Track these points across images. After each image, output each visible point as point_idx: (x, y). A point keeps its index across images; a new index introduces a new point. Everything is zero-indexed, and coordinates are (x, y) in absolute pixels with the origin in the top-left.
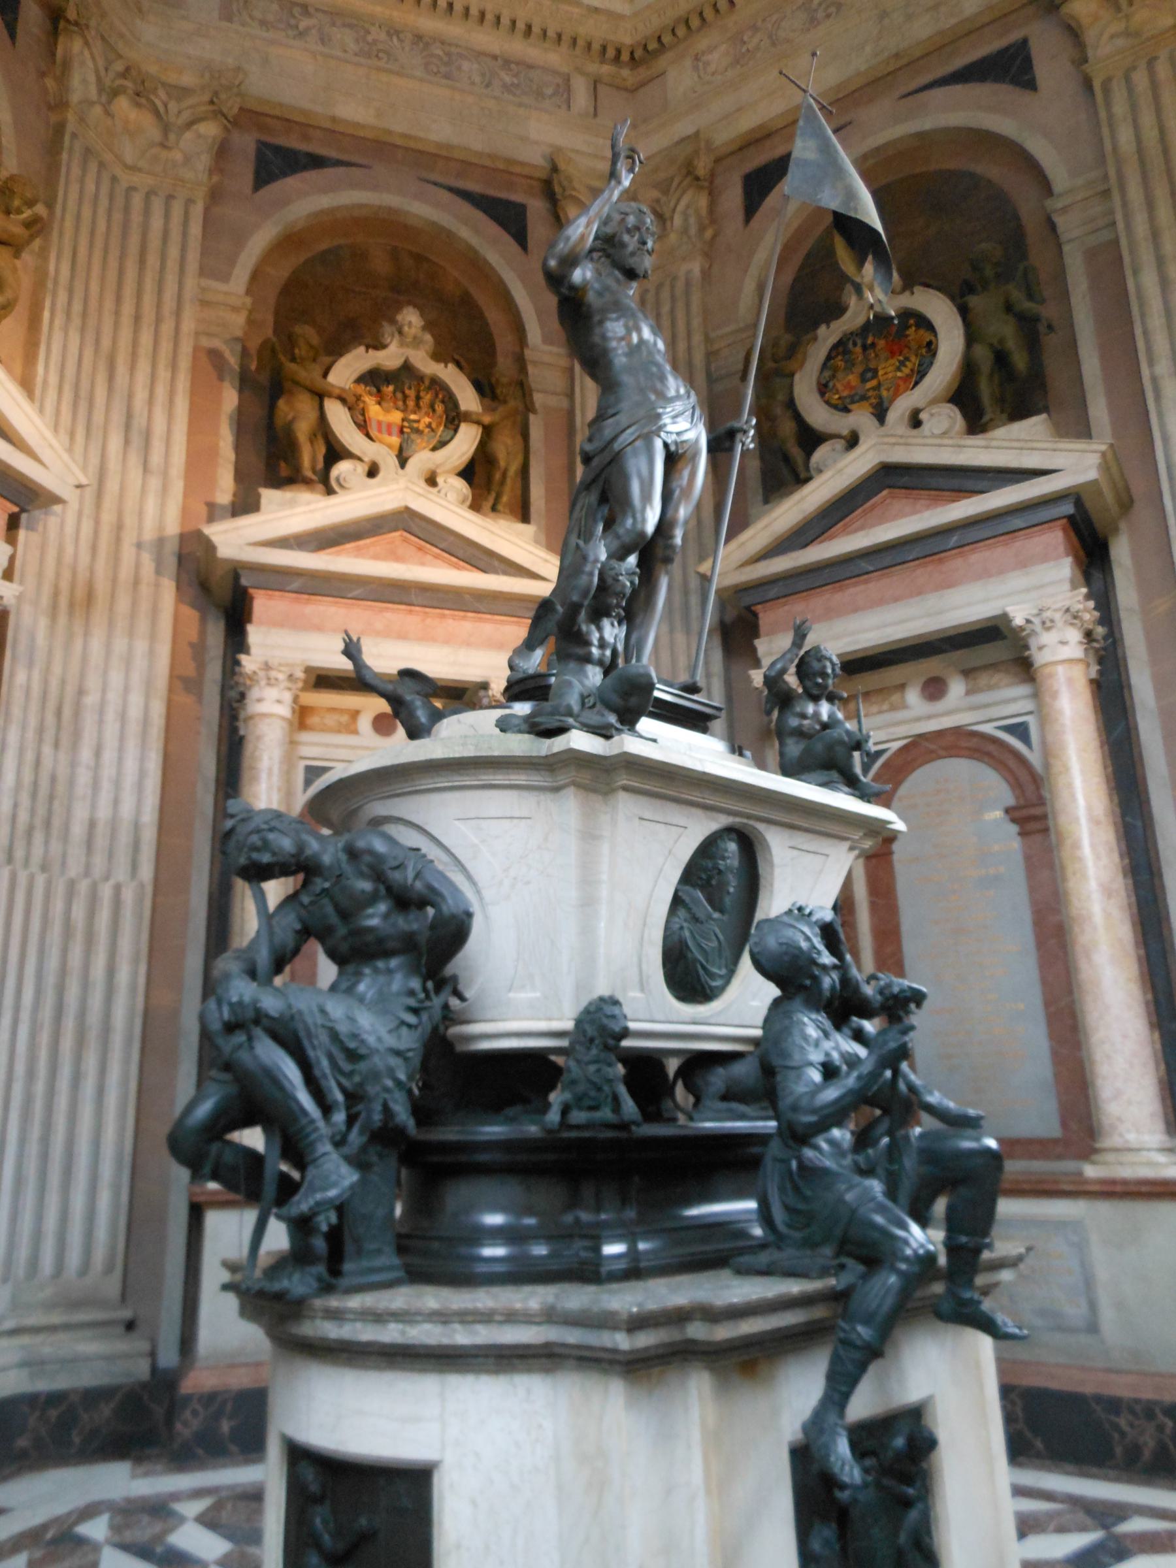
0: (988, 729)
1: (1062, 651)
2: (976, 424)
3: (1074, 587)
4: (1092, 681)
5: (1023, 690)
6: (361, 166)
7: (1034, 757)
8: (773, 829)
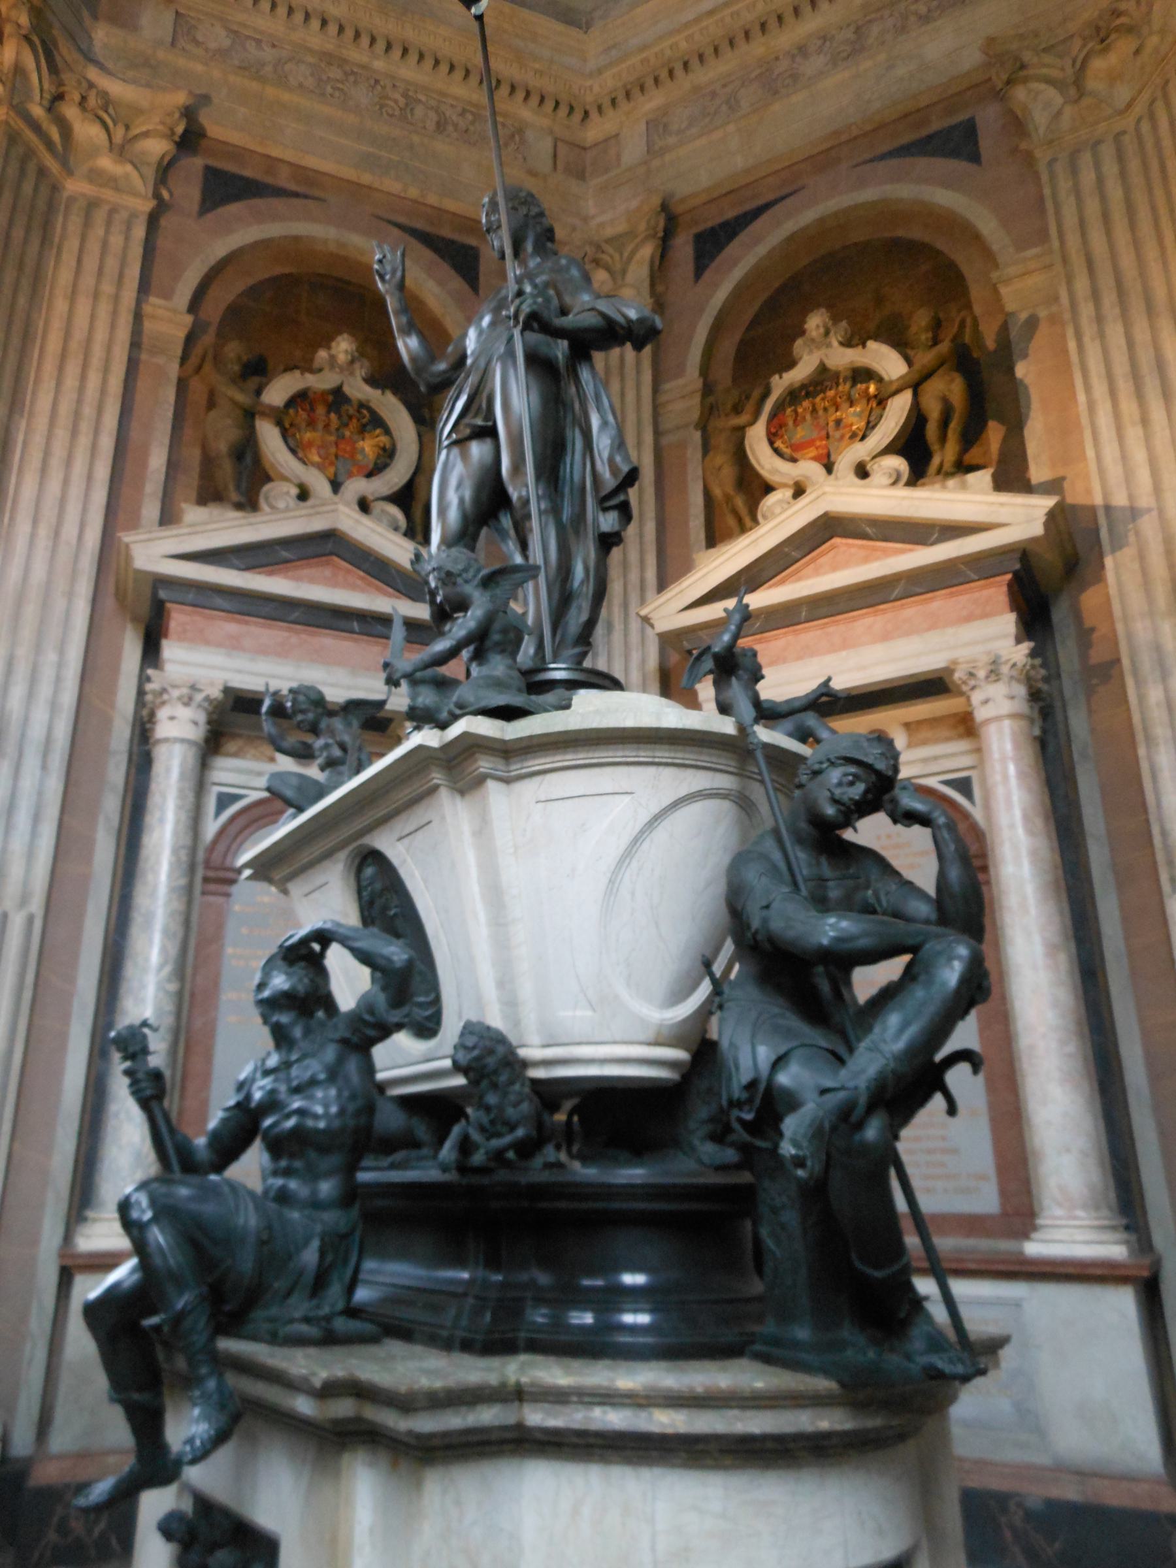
0: (932, 782)
1: (999, 707)
2: (917, 475)
3: (1019, 641)
4: (1035, 738)
5: (963, 745)
6: (296, 195)
7: (977, 813)
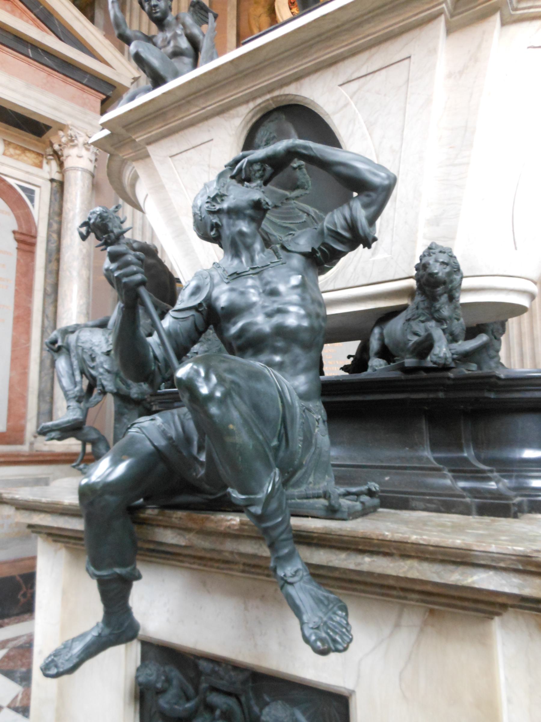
8: (306, 81)
